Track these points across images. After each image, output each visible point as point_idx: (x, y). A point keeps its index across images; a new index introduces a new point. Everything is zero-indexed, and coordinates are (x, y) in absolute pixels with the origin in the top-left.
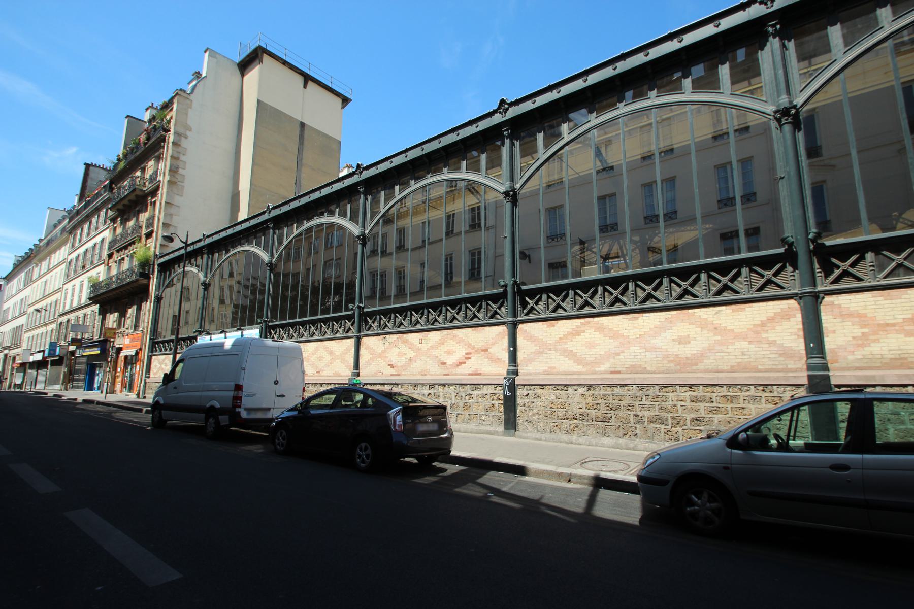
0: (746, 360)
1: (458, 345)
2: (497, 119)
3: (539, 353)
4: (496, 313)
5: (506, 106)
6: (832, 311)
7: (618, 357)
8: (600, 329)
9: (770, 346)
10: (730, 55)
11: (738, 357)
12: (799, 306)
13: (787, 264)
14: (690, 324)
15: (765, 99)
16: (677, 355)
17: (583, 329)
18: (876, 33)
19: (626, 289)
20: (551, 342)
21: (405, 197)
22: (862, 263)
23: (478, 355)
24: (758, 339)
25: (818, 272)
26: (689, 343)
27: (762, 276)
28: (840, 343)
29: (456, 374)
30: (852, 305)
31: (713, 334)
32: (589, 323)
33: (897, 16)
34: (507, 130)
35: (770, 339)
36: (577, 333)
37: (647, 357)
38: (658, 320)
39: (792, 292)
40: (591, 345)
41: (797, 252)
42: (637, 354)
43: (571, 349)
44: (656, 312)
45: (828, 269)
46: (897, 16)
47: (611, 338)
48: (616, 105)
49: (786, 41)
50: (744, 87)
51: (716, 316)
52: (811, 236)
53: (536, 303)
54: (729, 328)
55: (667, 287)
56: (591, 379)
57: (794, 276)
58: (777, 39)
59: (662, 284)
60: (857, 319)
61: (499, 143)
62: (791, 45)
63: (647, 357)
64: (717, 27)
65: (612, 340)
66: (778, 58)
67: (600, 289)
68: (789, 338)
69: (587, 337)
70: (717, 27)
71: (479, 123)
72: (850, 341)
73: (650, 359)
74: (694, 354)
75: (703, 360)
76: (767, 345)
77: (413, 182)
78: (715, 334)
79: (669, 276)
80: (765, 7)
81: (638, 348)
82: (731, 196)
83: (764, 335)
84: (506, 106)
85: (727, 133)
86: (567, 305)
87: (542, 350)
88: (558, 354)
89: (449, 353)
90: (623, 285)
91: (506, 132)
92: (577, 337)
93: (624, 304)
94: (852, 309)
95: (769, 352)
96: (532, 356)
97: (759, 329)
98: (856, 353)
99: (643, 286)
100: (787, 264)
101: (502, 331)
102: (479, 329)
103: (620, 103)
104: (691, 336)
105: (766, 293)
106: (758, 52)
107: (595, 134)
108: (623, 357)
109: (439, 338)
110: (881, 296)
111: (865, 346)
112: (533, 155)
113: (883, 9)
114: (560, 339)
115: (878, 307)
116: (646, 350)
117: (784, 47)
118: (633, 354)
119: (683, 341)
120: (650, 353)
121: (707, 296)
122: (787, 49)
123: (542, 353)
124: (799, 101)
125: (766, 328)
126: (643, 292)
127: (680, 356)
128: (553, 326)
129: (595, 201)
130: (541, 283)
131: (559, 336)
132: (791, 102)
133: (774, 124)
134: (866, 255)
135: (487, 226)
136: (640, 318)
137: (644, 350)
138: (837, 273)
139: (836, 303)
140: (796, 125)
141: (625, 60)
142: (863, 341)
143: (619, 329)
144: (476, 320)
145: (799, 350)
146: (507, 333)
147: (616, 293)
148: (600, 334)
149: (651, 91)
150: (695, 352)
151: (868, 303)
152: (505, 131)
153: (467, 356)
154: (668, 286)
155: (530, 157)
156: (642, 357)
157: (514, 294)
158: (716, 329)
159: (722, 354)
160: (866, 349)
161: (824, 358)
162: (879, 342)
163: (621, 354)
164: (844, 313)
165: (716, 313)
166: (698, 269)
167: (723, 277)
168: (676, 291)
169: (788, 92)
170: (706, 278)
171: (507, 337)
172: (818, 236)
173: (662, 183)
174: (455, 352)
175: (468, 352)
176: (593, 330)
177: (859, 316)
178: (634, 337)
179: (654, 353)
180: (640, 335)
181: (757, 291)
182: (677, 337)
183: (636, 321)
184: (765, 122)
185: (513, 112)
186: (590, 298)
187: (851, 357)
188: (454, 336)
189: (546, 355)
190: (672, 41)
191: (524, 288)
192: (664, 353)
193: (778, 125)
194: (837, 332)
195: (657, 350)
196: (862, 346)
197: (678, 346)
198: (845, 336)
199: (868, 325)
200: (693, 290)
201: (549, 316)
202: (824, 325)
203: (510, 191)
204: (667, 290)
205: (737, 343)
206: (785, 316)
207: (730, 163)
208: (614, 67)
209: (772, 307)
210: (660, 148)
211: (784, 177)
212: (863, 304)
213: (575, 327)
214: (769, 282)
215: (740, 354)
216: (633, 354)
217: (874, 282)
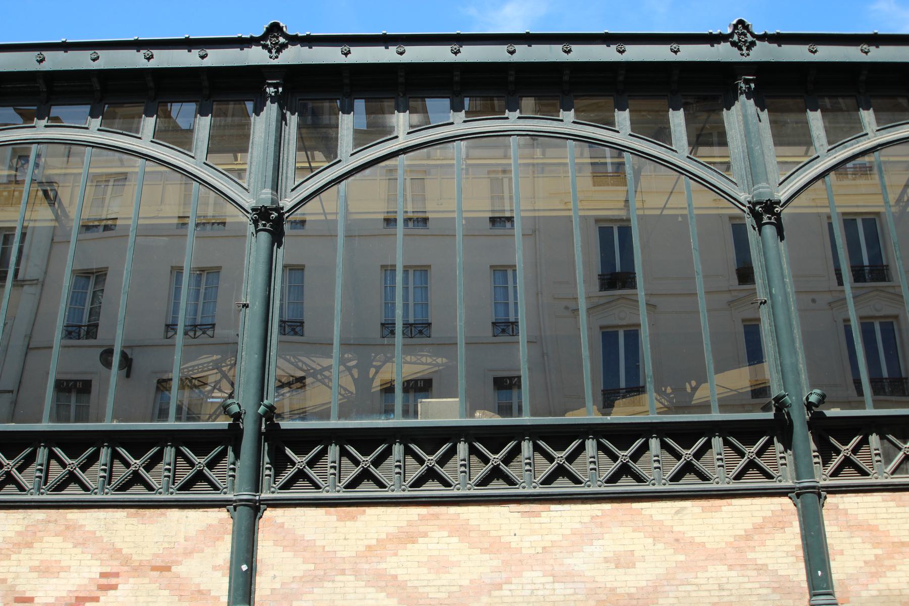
0: (726, 599)
1: (78, 550)
2: (257, 56)
3: (314, 579)
4: (200, 477)
5: (282, 40)
6: (837, 519)
7: (496, 593)
8: (462, 531)
9: (759, 575)
11: (713, 593)
12: (796, 508)
13: (775, 439)
14: (634, 531)
16: (613, 589)
17: (422, 529)
18: (861, 138)
19: (157, 458)
20: (345, 554)
22: (865, 447)
23: (139, 580)
24: (741, 562)
25: (267, 468)
26: (634, 566)
28: (850, 571)
30: (861, 511)
31: (672, 551)
32: (436, 516)
34: (276, 86)
35: (759, 562)
36: (409, 537)
37: (557, 592)
38: (578, 519)
39: (783, 484)
40: (440, 565)
41: (243, 430)
42: (537, 586)
43: (393, 572)
44: (575, 503)
45: (280, 463)
47: (484, 551)
48: (504, 113)
49: (288, 113)
50: (223, 160)
51: (676, 517)
53: (311, 464)
54: (697, 540)
55: (105, 465)
57: (784, 458)
58: (275, 105)
59: (584, 449)
60: (868, 534)
61: (250, 106)
62: (293, 120)
63: (557, 592)
65: (487, 556)
67: (105, 454)
68: (785, 560)
69: (430, 546)
71: (210, 52)
72: (861, 567)
73: (562, 598)
74: (642, 588)
75: (657, 598)
76: (754, 573)
77: (867, 117)
78: (676, 551)
79: (49, 446)
80: (739, 52)
81: (540, 574)
82: (512, 319)
83: (751, 555)
84: (282, 40)
85: (510, 219)
87: (322, 573)
88: (363, 584)
89: (45, 570)
90: (90, 450)
91: (272, 89)
92: (409, 546)
93: (150, 488)
94: (860, 517)
95: (757, 585)
96: (294, 586)
97: (742, 544)
98: (870, 587)
99: (549, 450)
100: (775, 439)
101: (215, 522)
102: (148, 512)
103: (39, 119)
104: (636, 554)
105: (747, 483)
106: (723, 110)
107: (464, 150)
108: (509, 593)
109: (18, 528)
110: (891, 501)
111: (881, 577)
113: (402, 114)
114: (369, 548)
115: (889, 516)
116: (556, 578)
117: (283, 118)
118: (529, 587)
119: (625, 561)
120: (562, 585)
121: (39, 489)
122: (286, 124)
123: (321, 580)
124: (287, 203)
125: (752, 544)
126: (546, 461)
127: (619, 591)
128: (353, 518)
129: (67, 281)
130: (39, 421)
131: (366, 542)
132: (273, 201)
133: (749, 221)
134: (870, 437)
135: (20, 277)
136: (543, 514)
137: (551, 579)
138: (290, 472)
139: (841, 507)
141: (242, 49)
142: (877, 567)
143: (500, 533)
144: (10, 488)
145: (799, 582)
146: (230, 527)
147: (136, 463)
148: (461, 541)
149: (147, 116)
150: (644, 584)
151: (878, 510)
152: (270, 85)
153: (104, 581)
154: (45, 462)
155: (232, 155)
156: (547, 592)
158: (678, 542)
159: (689, 588)
160: (882, 580)
162: (895, 570)
163: (505, 586)
164: (851, 523)
165: (677, 513)
167: (684, 448)
168: (415, 471)
169: (275, 187)
170: (45, 457)
171: (228, 539)
173: (283, 271)
174: (67, 569)
175: (108, 570)
176: (446, 534)
177: (872, 529)
178: (532, 551)
179: (571, 585)
180: (544, 548)
181: (608, 482)
182: (611, 555)
183: (537, 520)
184: (242, 223)
185: (293, 56)
186: (438, 462)
187: (864, 594)
188: (68, 527)
189: (330, 585)
190: (138, 51)
191: (285, 425)
192: (588, 585)
194: (845, 553)
195: (576, 579)
196: (875, 575)
197: (615, 571)
198: (855, 560)
199: (881, 543)
200: (572, 468)
201: (341, 495)
202: (829, 541)
205: (710, 568)
206: (777, 523)
207: (513, 267)
208: (203, 53)
209: (758, 508)
210: (406, 212)
211: (765, 302)
212: (872, 511)
213: (404, 524)
215: (716, 587)
216: (529, 587)
217: (463, 489)
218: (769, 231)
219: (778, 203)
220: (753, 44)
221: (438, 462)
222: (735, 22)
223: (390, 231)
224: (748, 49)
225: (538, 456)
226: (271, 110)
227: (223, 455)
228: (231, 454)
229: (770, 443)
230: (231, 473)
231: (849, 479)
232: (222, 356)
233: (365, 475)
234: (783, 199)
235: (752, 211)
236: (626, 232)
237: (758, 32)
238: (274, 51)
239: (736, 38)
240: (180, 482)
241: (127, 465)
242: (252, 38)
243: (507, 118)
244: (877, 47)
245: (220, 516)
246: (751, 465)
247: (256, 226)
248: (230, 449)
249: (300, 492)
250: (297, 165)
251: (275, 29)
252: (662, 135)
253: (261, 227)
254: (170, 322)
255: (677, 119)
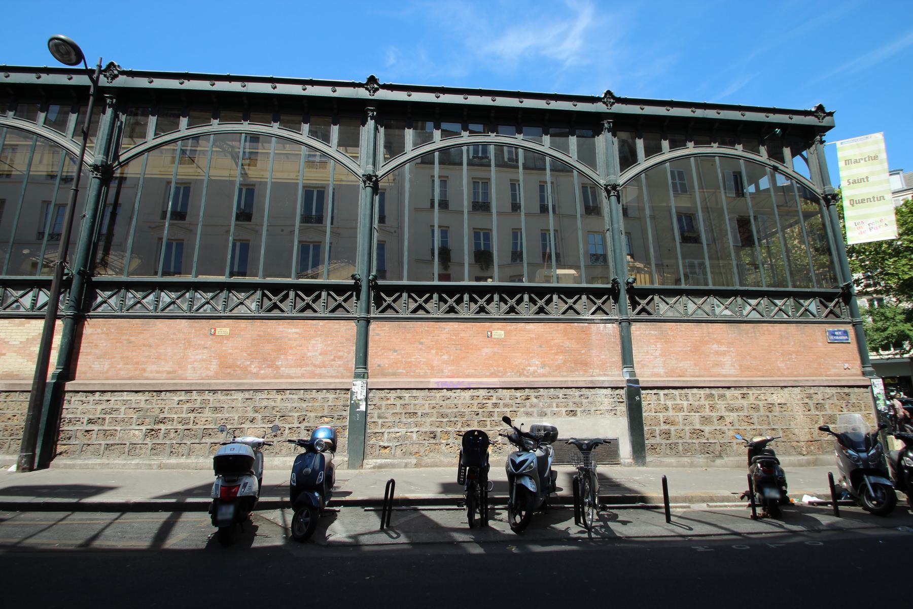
2: (600, 107)
5: (376, 86)
10: (420, 124)
13: (611, 297)
15: (92, 153)
19: (286, 297)
21: (196, 137)
27: (566, 303)
29: (719, 375)
33: (190, 125)
45: (379, 301)
46: (190, 125)
48: (270, 123)
49: (121, 114)
50: (341, 149)
52: (371, 277)
56: (831, 380)
64: (274, 88)
66: (372, 136)
70: (274, 88)
79: (262, 290)
84: (376, 86)
86: (491, 307)
93: (282, 311)
100: (611, 297)
112: (348, 148)
117: (376, 129)
124: (380, 173)
128: (23, 325)
132: (374, 172)
138: (385, 304)
140: (375, 189)
157: (370, 288)
161: (633, 367)
166: (321, 287)
169: (374, 164)
172: (375, 278)
193: (606, 195)
200: (314, 306)
203: (373, 176)
204: (292, 302)
214: (340, 306)
218: (613, 199)
219: (619, 185)
220: (824, 117)
221: (424, 301)
222: (605, 92)
223: (51, 182)
224: (611, 106)
225: (560, 301)
226: (371, 123)
227: (351, 296)
228: (354, 298)
229: (608, 299)
230: (556, 307)
231: (644, 316)
232: (30, 250)
233: (420, 307)
234: (621, 183)
235: (606, 189)
236: (321, 193)
237: (381, 83)
238: (372, 91)
239: (605, 100)
240: (330, 308)
241: (270, 300)
242: (360, 83)
243: (712, 147)
244: (189, 81)
245: (353, 324)
246: (571, 308)
247: (365, 184)
248: (355, 293)
249: (389, 314)
250: (276, 152)
251: (372, 80)
252: (326, 139)
253: (367, 185)
254: (41, 231)
255: (335, 130)
